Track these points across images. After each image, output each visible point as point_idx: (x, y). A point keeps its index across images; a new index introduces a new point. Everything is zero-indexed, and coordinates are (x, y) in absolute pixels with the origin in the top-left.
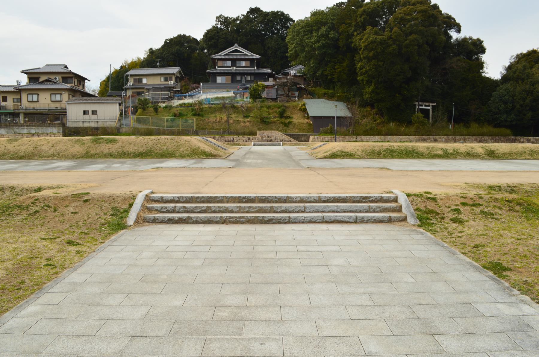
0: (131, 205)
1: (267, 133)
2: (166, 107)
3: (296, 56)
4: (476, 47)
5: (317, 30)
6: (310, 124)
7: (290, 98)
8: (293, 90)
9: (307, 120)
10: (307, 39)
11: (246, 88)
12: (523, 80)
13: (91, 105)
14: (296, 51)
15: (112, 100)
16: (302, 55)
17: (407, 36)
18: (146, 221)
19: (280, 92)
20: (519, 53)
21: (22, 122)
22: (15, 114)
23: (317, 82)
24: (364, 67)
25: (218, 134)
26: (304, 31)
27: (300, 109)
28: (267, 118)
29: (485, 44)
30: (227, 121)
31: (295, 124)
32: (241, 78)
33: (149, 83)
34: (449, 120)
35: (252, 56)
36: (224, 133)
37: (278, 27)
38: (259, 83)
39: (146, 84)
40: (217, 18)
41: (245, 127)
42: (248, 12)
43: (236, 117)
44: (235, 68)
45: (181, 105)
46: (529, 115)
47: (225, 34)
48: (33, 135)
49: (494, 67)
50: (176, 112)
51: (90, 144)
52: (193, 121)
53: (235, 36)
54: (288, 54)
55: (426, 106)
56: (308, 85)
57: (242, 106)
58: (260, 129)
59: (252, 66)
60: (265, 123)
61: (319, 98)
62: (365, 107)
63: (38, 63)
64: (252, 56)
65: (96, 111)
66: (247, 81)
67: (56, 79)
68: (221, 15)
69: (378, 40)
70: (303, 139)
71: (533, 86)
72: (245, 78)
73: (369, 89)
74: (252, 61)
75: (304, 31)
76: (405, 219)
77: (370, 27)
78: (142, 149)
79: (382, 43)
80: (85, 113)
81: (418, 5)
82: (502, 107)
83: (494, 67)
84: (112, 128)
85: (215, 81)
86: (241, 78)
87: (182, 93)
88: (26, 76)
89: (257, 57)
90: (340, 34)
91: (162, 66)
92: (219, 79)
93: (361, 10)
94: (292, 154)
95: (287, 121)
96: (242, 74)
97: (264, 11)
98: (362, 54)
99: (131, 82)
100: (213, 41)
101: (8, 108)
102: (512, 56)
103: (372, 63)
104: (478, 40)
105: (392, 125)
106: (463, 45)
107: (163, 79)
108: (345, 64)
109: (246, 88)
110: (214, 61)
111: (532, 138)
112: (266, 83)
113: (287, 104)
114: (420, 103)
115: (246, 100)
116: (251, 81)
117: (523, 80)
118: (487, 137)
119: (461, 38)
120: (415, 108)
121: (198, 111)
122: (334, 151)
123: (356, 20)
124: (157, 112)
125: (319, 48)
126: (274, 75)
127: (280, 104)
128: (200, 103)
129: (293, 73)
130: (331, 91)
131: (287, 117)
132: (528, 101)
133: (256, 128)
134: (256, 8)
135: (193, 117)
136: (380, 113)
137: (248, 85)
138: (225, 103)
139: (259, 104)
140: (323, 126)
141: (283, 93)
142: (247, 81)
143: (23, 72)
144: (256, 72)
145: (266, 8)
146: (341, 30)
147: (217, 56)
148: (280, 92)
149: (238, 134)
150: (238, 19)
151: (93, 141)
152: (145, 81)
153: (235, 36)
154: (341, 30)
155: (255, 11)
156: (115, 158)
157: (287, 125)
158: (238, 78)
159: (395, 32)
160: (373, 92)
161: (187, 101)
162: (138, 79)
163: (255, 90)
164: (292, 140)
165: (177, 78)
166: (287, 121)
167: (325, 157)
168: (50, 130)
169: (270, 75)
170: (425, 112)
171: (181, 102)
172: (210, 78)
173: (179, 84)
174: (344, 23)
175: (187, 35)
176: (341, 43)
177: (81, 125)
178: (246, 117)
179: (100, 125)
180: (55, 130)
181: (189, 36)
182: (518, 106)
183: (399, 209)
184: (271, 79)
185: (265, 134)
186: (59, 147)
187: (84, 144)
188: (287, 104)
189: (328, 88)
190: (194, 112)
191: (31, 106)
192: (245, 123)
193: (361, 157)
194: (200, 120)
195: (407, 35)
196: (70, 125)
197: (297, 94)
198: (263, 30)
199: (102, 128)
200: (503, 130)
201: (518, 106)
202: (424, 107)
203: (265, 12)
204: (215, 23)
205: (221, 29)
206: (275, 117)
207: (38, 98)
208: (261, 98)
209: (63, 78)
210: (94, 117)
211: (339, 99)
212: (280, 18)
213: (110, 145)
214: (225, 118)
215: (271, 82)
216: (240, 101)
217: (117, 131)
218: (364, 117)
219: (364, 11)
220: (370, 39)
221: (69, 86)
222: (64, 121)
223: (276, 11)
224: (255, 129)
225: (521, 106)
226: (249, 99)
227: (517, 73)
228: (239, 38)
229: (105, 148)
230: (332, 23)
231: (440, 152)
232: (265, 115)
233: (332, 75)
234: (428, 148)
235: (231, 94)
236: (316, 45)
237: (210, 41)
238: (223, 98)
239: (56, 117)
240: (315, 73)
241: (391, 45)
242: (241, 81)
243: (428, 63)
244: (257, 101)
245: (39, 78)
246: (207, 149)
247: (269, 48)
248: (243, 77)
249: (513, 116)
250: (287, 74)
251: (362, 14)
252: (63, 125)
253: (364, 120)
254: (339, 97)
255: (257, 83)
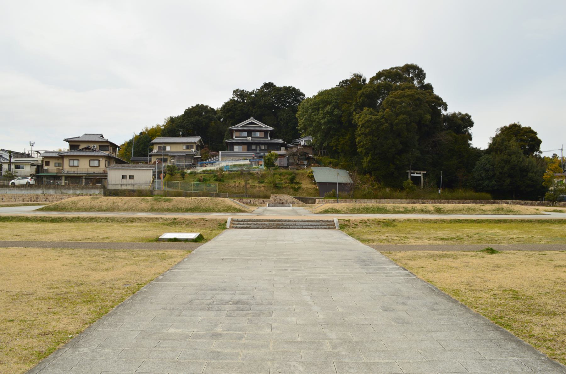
0: (226, 222)
1: (279, 196)
2: (191, 173)
3: (305, 128)
4: (465, 121)
5: (323, 108)
6: (317, 189)
7: (299, 166)
8: (302, 159)
9: (314, 186)
10: (314, 115)
11: (261, 157)
12: (501, 151)
13: (129, 171)
14: (305, 125)
15: (147, 167)
16: (310, 129)
17: (397, 116)
18: (233, 227)
19: (290, 161)
20: (503, 126)
21: (63, 184)
22: (57, 177)
23: (324, 152)
24: (362, 141)
25: (237, 197)
26: (312, 109)
27: (308, 176)
28: (279, 183)
29: (473, 119)
30: (245, 186)
31: (303, 189)
32: (256, 148)
33: (173, 150)
34: (439, 187)
35: (266, 127)
36: (242, 196)
37: (290, 100)
38: (273, 152)
39: (169, 152)
40: (234, 92)
41: (260, 191)
42: (262, 87)
43: (252, 182)
44: (250, 138)
45: (204, 172)
46: (508, 181)
47: (243, 106)
48: (78, 195)
49: (481, 139)
50: (201, 178)
51: (153, 202)
52: (216, 186)
53: (251, 108)
54: (298, 128)
55: (417, 173)
56: (316, 154)
57: (257, 173)
58: (273, 193)
59: (266, 136)
60: (277, 188)
61: (325, 166)
62: (365, 174)
63: (77, 133)
64: (266, 127)
65: (133, 176)
66: (261, 150)
67: (94, 147)
68: (237, 90)
69: (373, 119)
70: (310, 202)
71: (510, 156)
72: (260, 148)
73: (366, 160)
74: (266, 132)
75: (312, 109)
76: (335, 228)
77: (367, 108)
78: (191, 206)
79: (376, 121)
80: (123, 177)
81: (407, 90)
82: (484, 174)
83: (481, 139)
84: (146, 190)
85: (233, 150)
86: (256, 148)
87: (202, 160)
88: (68, 144)
89: (271, 128)
90: (343, 112)
91: (183, 135)
92: (236, 148)
93: (360, 92)
94: (298, 211)
95: (297, 186)
96: (257, 144)
97: (277, 86)
98: (359, 131)
99: (156, 150)
100: (230, 113)
101: (50, 171)
102: (498, 129)
103: (368, 138)
104: (467, 115)
105: (388, 190)
106: (453, 120)
107: (185, 147)
108: (347, 137)
109: (261, 157)
110: (232, 132)
111: (509, 201)
112: (279, 153)
113: (297, 172)
114: (412, 172)
115: (260, 168)
116: (264, 150)
117: (501, 151)
118: (469, 201)
119: (451, 114)
120: (408, 176)
121: (220, 177)
122: (327, 208)
123: (356, 100)
124: (183, 177)
125: (325, 123)
126: (286, 144)
127: (291, 171)
128: (221, 170)
129: (302, 143)
130: (335, 161)
131: (297, 183)
132: (506, 169)
133: (270, 192)
134: (270, 83)
135: (215, 182)
136: (378, 180)
137: (262, 154)
138: (243, 170)
139: (273, 172)
140: (327, 190)
141: (293, 161)
142: (261, 150)
143: (66, 140)
144: (270, 142)
145: (279, 83)
146: (343, 108)
147: (234, 128)
148: (290, 161)
149: (254, 197)
150: (253, 92)
151: (155, 200)
152: (168, 148)
153: (251, 108)
154: (343, 108)
155: (268, 86)
156: (172, 212)
157: (296, 190)
158: (254, 147)
159: (387, 113)
160: (370, 162)
161: (209, 168)
162: (162, 147)
163: (269, 159)
164: (301, 202)
165: (197, 146)
166: (297, 186)
167: (320, 213)
168: (92, 191)
169: (282, 145)
170: (416, 180)
171: (204, 169)
172: (229, 147)
173: (199, 151)
174: (346, 103)
175: (205, 105)
176: (343, 119)
177: (119, 187)
178: (261, 182)
179: (135, 188)
180: (97, 192)
181: (207, 106)
182: (498, 174)
183: (334, 225)
184: (283, 149)
185: (278, 197)
186: (130, 204)
187: (148, 202)
188: (297, 172)
189: (334, 158)
190: (216, 178)
191: (71, 170)
192: (260, 188)
193: (345, 213)
194: (221, 183)
195: (397, 115)
196: (110, 187)
197: (305, 162)
198: (276, 103)
199: (138, 190)
200: (483, 194)
201: (498, 174)
202: (415, 175)
203: (278, 87)
204: (232, 96)
205: (237, 101)
206: (286, 183)
207: (79, 163)
208: (274, 165)
209: (100, 146)
210: (131, 181)
211: (343, 167)
212: (292, 93)
213: (167, 203)
214: (243, 183)
215: (283, 151)
216: (256, 168)
217: (150, 193)
218: (364, 183)
219: (363, 93)
220: (366, 119)
221: (106, 153)
222: (105, 184)
223: (288, 86)
224: (269, 193)
225: (501, 173)
226: (263, 167)
227: (497, 145)
228: (254, 111)
229: (165, 205)
230: (336, 102)
231: (402, 210)
232: (277, 181)
233: (336, 146)
234: (394, 207)
235: (247, 162)
236: (323, 121)
237: (227, 112)
238: (240, 166)
239: (97, 180)
240: (322, 143)
241: (384, 123)
242: (256, 150)
243: (417, 137)
244: (271, 168)
245: (79, 146)
246: (237, 207)
247: (281, 119)
248: (258, 147)
249: (494, 182)
250: (298, 144)
251: (361, 96)
252: (104, 187)
253: (364, 186)
254: (342, 165)
255: (270, 152)
